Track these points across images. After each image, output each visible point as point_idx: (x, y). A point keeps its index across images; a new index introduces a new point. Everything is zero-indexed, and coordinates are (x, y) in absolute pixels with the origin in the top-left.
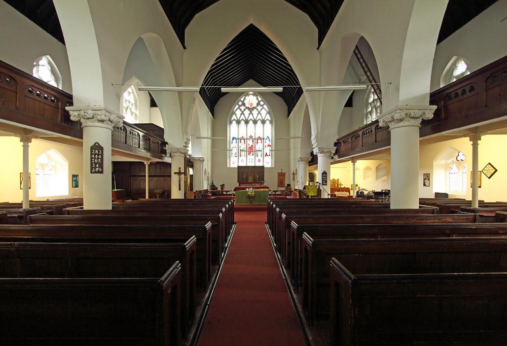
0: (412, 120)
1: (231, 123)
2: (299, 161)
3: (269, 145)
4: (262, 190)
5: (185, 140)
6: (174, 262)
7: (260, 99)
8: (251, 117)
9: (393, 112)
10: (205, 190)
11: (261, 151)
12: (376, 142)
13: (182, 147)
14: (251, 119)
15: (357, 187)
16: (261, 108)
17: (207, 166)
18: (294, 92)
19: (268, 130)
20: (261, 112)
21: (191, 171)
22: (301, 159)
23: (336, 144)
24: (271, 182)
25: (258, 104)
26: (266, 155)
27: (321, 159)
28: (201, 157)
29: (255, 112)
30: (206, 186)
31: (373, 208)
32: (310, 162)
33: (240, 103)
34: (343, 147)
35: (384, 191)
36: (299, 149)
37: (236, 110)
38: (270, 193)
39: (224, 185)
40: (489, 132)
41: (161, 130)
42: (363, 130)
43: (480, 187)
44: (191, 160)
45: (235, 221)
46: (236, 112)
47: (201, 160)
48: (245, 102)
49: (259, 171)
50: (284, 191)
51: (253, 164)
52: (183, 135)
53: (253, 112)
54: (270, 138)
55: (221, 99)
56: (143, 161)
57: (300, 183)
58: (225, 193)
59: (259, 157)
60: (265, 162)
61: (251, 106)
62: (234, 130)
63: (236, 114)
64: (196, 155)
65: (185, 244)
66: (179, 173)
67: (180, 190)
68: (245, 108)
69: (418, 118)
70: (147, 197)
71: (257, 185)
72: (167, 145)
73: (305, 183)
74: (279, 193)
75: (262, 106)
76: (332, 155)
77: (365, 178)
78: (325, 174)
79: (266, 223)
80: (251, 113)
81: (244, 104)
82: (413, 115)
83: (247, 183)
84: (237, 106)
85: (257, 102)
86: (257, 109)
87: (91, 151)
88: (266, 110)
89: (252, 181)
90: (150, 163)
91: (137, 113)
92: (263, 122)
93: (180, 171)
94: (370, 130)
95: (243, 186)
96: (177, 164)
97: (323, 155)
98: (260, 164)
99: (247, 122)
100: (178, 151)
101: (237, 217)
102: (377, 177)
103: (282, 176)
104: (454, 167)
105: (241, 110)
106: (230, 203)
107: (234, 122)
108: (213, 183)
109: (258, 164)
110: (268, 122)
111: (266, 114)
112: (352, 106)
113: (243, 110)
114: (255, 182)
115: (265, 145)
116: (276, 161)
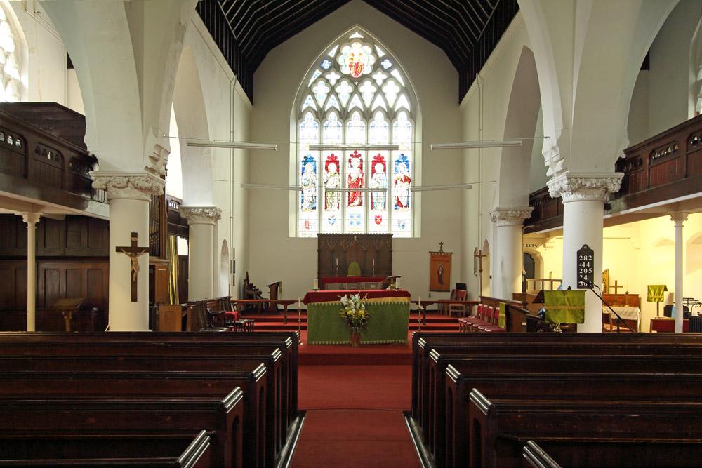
1: (300, 116)
2: (494, 219)
3: (407, 179)
4: (390, 300)
5: (151, 151)
6: (259, 365)
7: (381, 53)
8: (356, 101)
10: (226, 298)
11: (384, 190)
13: (142, 170)
14: (356, 108)
15: (666, 294)
16: (385, 76)
17: (230, 231)
18: (481, 27)
19: (405, 135)
20: (385, 89)
21: (183, 247)
22: (503, 215)
23: (620, 165)
24: (411, 276)
25: (377, 67)
26: (399, 204)
27: (573, 209)
28: (211, 205)
29: (367, 88)
30: (225, 287)
32: (526, 222)
33: (326, 64)
34: (647, 174)
36: (496, 187)
37: (315, 82)
38: (414, 307)
39: (278, 284)
40: (697, 210)
41: (78, 121)
44: (182, 215)
45: (300, 407)
46: (314, 89)
47: (213, 216)
48: (340, 60)
49: (377, 249)
50: (448, 303)
51: (360, 230)
52: (145, 135)
53: (361, 89)
54: (410, 159)
55: (271, 52)
56: (17, 213)
57: (498, 282)
58: (281, 307)
59: (379, 211)
60: (394, 223)
61: (356, 73)
62: (305, 134)
63: (313, 94)
64: (196, 200)
65: (224, 401)
66: (134, 250)
67: (134, 298)
68: (338, 77)
70: (31, 327)
71: (373, 287)
72: (96, 168)
73: (513, 280)
74: (434, 307)
75: (388, 71)
78: (586, 258)
79: (407, 414)
80: (356, 91)
81: (336, 67)
83: (343, 279)
84: (318, 73)
85: (373, 60)
86: (374, 82)
87: (578, 258)
88: (397, 82)
89: (359, 275)
90: (42, 218)
91: (25, 80)
92: (391, 115)
93: (134, 243)
95: (332, 289)
96: (126, 222)
97: (580, 197)
98: (382, 229)
99: (344, 115)
100: (129, 182)
101: (310, 387)
103: (440, 263)
105: (328, 81)
106: (288, 342)
107: (309, 117)
108: (247, 280)
109: (374, 229)
110: (403, 117)
111: (399, 94)
112: (649, 69)
113: (333, 82)
114: (365, 277)
115: (394, 177)
116: (427, 222)
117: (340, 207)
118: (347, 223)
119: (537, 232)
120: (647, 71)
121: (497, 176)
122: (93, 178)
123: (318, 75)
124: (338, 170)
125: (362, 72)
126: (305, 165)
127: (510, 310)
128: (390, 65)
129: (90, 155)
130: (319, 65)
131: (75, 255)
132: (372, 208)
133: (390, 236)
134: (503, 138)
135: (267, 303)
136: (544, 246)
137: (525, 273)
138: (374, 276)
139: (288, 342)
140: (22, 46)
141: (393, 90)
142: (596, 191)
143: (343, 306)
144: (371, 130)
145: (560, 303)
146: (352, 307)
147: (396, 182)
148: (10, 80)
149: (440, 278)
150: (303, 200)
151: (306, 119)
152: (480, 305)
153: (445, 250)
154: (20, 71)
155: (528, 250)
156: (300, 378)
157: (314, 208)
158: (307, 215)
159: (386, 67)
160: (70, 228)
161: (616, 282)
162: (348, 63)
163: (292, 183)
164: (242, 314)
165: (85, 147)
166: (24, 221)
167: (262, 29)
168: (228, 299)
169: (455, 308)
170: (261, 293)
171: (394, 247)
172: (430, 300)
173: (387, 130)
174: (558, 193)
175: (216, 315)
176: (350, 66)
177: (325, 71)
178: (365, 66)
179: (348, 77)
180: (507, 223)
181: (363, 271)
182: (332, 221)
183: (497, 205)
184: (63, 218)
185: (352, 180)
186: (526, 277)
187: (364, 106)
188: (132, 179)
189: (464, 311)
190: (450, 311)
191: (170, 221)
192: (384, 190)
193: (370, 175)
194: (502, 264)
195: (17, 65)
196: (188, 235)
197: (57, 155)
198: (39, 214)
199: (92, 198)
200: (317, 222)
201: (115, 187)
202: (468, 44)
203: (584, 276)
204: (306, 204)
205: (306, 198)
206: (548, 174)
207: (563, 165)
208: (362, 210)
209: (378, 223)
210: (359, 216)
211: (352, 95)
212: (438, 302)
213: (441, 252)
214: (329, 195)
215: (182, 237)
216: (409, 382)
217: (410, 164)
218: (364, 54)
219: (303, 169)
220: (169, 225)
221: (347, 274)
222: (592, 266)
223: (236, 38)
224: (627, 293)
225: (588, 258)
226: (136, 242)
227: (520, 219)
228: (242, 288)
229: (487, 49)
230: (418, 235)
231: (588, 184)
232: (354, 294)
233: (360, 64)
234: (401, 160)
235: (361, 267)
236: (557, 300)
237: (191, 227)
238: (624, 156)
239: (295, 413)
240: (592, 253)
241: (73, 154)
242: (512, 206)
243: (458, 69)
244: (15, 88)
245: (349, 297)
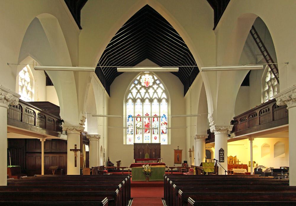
1: (127, 101)
2: (195, 139)
7: (156, 78)
11: (157, 128)
12: (273, 120)
16: (157, 86)
17: (103, 143)
18: (191, 71)
19: (164, 109)
20: (157, 91)
21: (87, 148)
22: (198, 137)
23: (232, 122)
24: (168, 160)
25: (154, 83)
26: (163, 132)
28: (97, 134)
29: (151, 91)
30: (102, 163)
32: (206, 140)
33: (136, 82)
34: (240, 126)
36: (196, 127)
37: (132, 89)
38: (166, 169)
39: (120, 161)
42: (260, 109)
44: (87, 137)
45: (131, 197)
46: (132, 91)
47: (98, 138)
50: (180, 168)
51: (149, 142)
52: (79, 113)
54: (167, 116)
55: (117, 78)
56: (38, 138)
57: (197, 160)
58: (121, 169)
59: (156, 135)
62: (129, 109)
66: (75, 150)
67: (76, 166)
68: (141, 87)
70: (43, 173)
71: (154, 162)
73: (202, 159)
74: (176, 169)
77: (263, 155)
78: (222, 152)
79: (163, 199)
80: (147, 92)
81: (140, 83)
83: (143, 159)
84: (133, 85)
85: (153, 81)
86: (153, 88)
87: (219, 152)
88: (162, 88)
89: (149, 158)
90: (46, 140)
92: (160, 100)
93: (76, 148)
94: (267, 109)
95: (139, 163)
96: (73, 141)
97: (219, 133)
98: (157, 141)
100: (74, 128)
101: (133, 192)
102: (276, 155)
103: (178, 153)
105: (137, 88)
107: (130, 101)
108: (109, 160)
110: (164, 101)
111: (162, 93)
113: (139, 89)
114: (151, 158)
115: (161, 123)
116: (173, 138)
117: (142, 133)
118: (144, 139)
119: (210, 143)
120: (249, 86)
121: (196, 124)
122: (62, 127)
123: (133, 86)
124: (141, 120)
125: (149, 85)
126: (129, 118)
127: (197, 169)
128: (159, 82)
129: (62, 119)
130: (134, 83)
131: (55, 151)
132: (153, 134)
133: (160, 144)
134: (197, 113)
135: (116, 168)
136: (214, 148)
137: (206, 157)
138: (154, 158)
139: (126, 179)
140: (32, 80)
141: (160, 92)
142: (225, 131)
143: (143, 168)
144: (152, 106)
145: (207, 166)
146: (146, 168)
147: (162, 125)
148: (29, 91)
149: (178, 159)
150: (128, 131)
151: (129, 102)
152: (191, 168)
153: (180, 149)
154: (32, 88)
155: (207, 149)
156: (131, 190)
157: (132, 134)
158: (130, 136)
159: (158, 83)
160: (53, 143)
161: (238, 160)
162: (144, 82)
163: (124, 126)
164: (109, 171)
165: (60, 117)
166: (41, 141)
167: (114, 73)
168: (103, 166)
169: (183, 169)
170: (114, 164)
171: (161, 148)
172: (174, 167)
173: (158, 106)
174: (213, 131)
175: (101, 172)
176: (145, 83)
177: (136, 85)
178: (150, 83)
179: (144, 87)
180: (200, 140)
181: (150, 156)
182: (139, 138)
183: (196, 134)
184: (51, 140)
185: (146, 123)
186: (206, 158)
187: (150, 97)
188: (75, 127)
189: (186, 171)
190: (181, 170)
191: (85, 140)
192: (157, 128)
193: (152, 122)
194: (198, 154)
195: (31, 86)
196: (89, 144)
197: (19, 106)
198: (45, 139)
199: (62, 133)
200: (133, 139)
201: (69, 130)
202: (186, 76)
203: (221, 158)
204: (129, 132)
205: (129, 130)
206: (210, 125)
207: (214, 123)
208: (149, 134)
209: (156, 139)
210: (148, 137)
211: (145, 93)
212: (177, 167)
213: (178, 150)
214: (138, 130)
215: (87, 145)
216: (163, 191)
217: (167, 118)
218: (150, 78)
219: (128, 120)
220: (83, 141)
221: (144, 157)
222: (224, 155)
223: (105, 75)
224: (242, 164)
225: (222, 152)
226: (76, 148)
227: (204, 139)
228: (107, 163)
229: (195, 75)
230: (170, 143)
231: (222, 129)
232: (147, 164)
233: (148, 82)
234: (164, 117)
235: (149, 155)
236: (206, 165)
237: (90, 141)
238: (233, 120)
239: (130, 198)
240: (224, 151)
241: (57, 120)
242: (201, 134)
243: (184, 85)
244: (30, 94)
245: (145, 165)
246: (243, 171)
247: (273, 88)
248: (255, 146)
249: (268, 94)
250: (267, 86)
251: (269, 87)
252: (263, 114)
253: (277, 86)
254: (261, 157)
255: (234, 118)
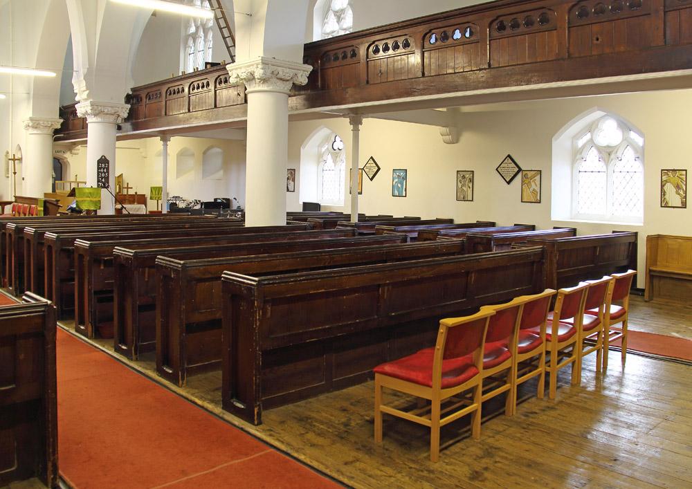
0: (280, 83)
9: (252, 65)
12: (216, 106)
23: (129, 99)
27: (95, 129)
31: (213, 227)
32: (56, 131)
35: (219, 201)
40: (370, 115)
42: (192, 80)
43: (360, 193)
69: (288, 80)
76: (119, 121)
77: (179, 173)
78: (103, 163)
82: (281, 75)
87: (98, 165)
94: (205, 82)
97: (99, 120)
102: (205, 173)
104: (329, 158)
224: (136, 193)
231: (106, 111)
238: (131, 93)
246: (139, 209)
247: (204, 32)
248: (159, 155)
249: (194, 42)
250: (193, 25)
251: (197, 28)
252: (196, 91)
253: (212, 30)
254: (177, 177)
255: (133, 90)
